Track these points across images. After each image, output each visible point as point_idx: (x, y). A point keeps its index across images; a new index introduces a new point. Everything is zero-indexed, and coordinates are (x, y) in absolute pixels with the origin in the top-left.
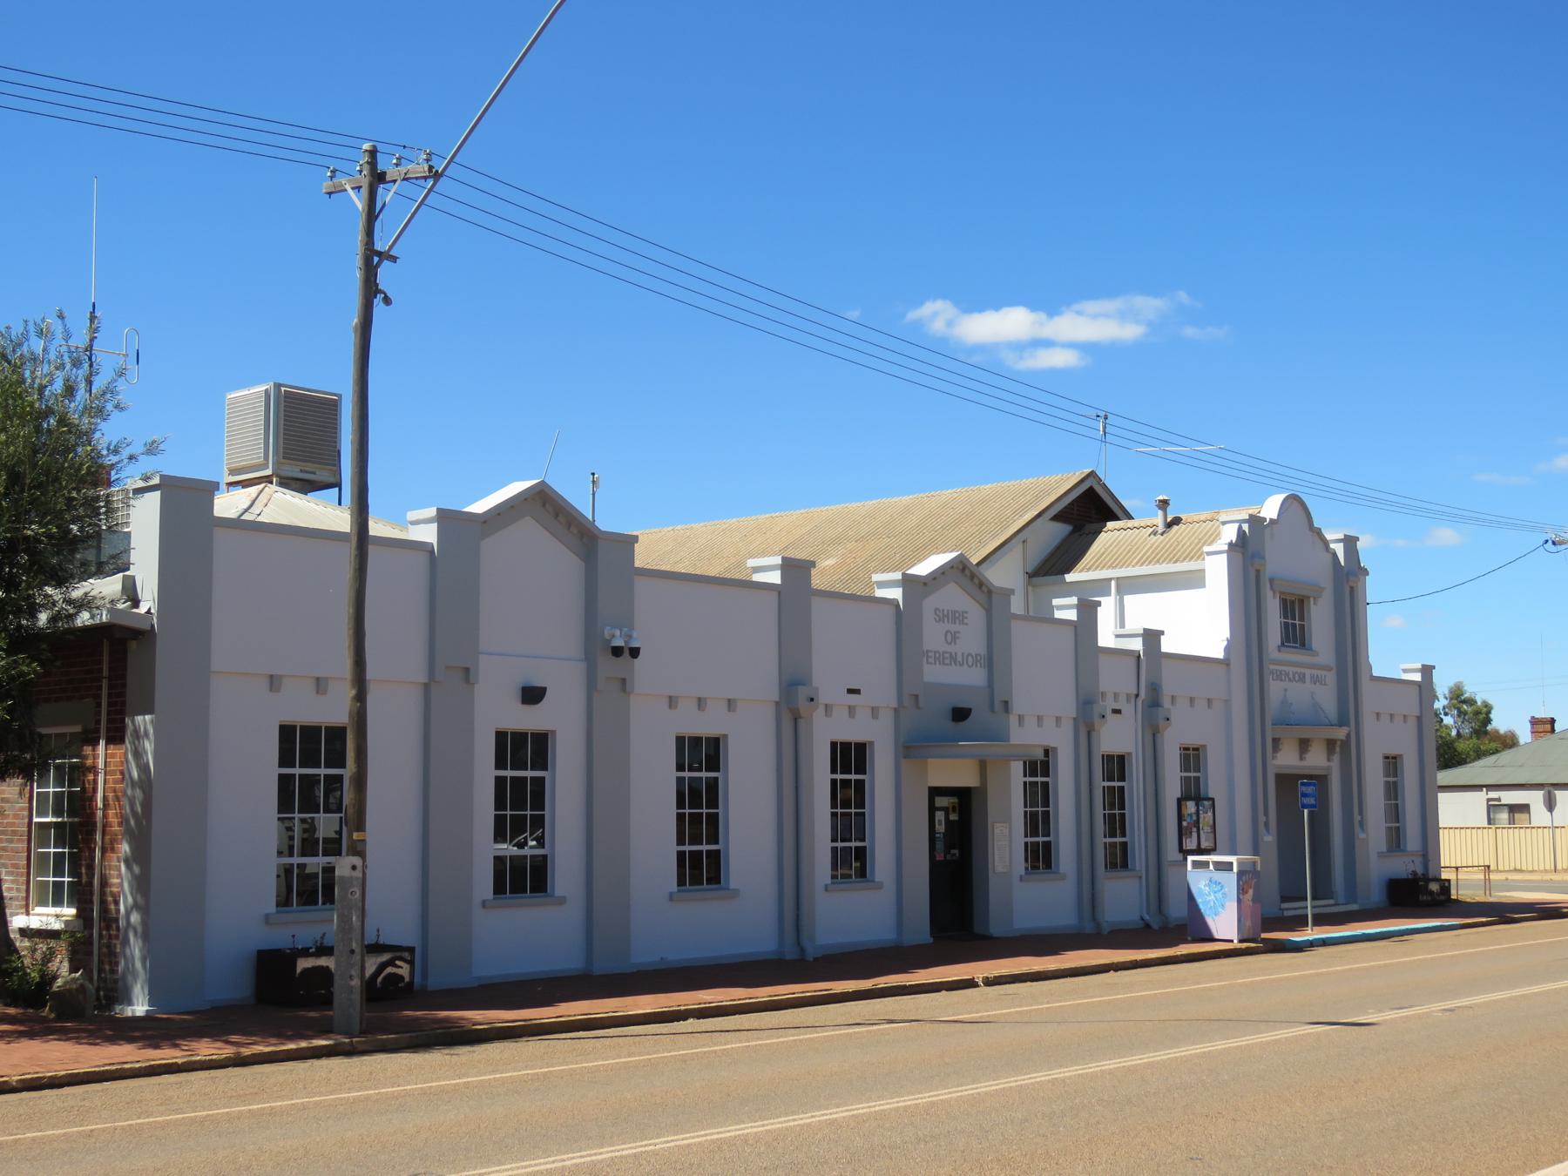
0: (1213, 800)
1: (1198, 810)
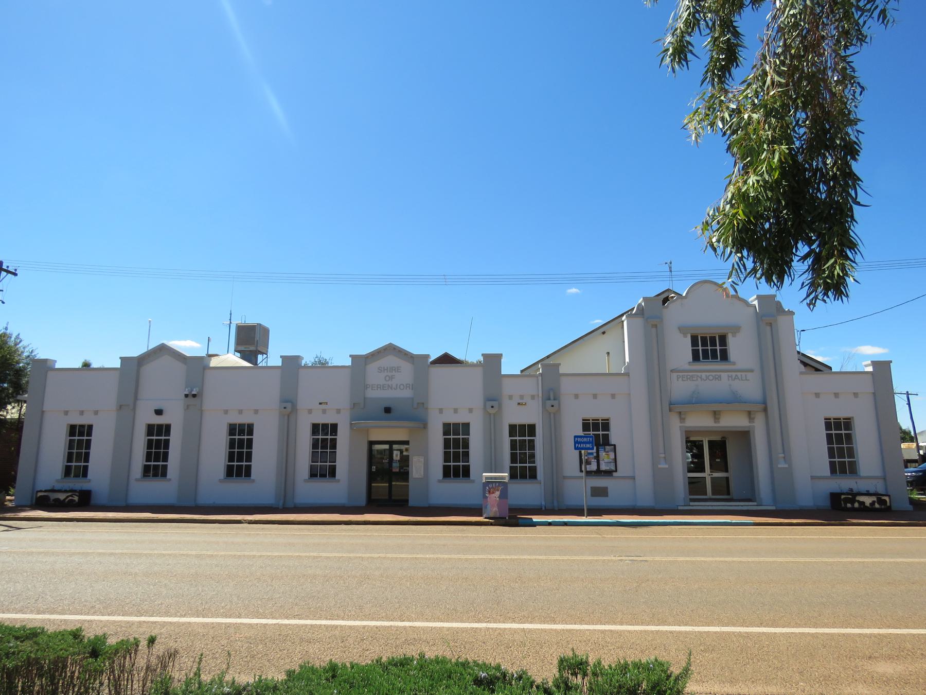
0: (615, 446)
1: (598, 452)
